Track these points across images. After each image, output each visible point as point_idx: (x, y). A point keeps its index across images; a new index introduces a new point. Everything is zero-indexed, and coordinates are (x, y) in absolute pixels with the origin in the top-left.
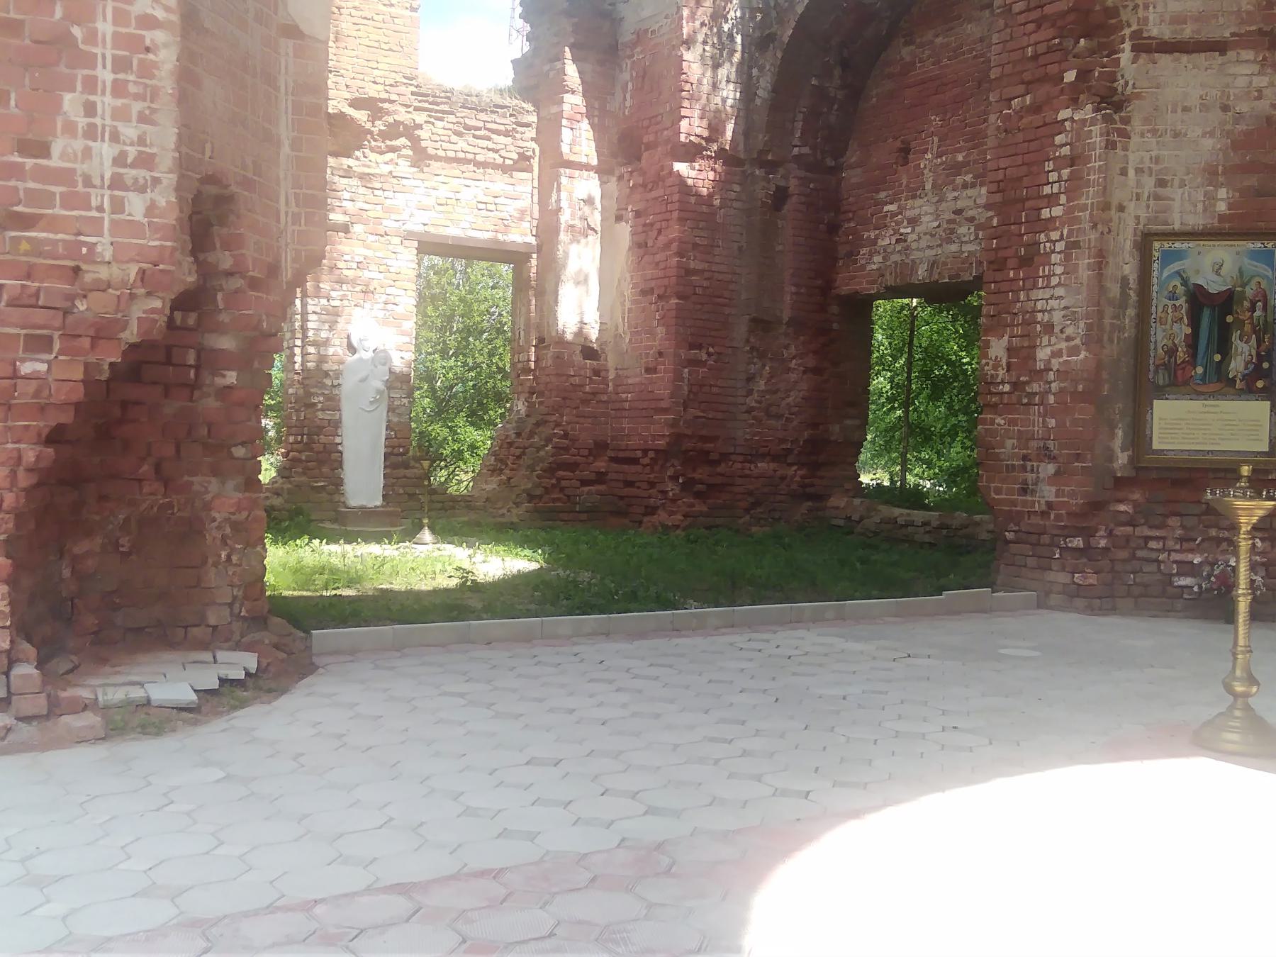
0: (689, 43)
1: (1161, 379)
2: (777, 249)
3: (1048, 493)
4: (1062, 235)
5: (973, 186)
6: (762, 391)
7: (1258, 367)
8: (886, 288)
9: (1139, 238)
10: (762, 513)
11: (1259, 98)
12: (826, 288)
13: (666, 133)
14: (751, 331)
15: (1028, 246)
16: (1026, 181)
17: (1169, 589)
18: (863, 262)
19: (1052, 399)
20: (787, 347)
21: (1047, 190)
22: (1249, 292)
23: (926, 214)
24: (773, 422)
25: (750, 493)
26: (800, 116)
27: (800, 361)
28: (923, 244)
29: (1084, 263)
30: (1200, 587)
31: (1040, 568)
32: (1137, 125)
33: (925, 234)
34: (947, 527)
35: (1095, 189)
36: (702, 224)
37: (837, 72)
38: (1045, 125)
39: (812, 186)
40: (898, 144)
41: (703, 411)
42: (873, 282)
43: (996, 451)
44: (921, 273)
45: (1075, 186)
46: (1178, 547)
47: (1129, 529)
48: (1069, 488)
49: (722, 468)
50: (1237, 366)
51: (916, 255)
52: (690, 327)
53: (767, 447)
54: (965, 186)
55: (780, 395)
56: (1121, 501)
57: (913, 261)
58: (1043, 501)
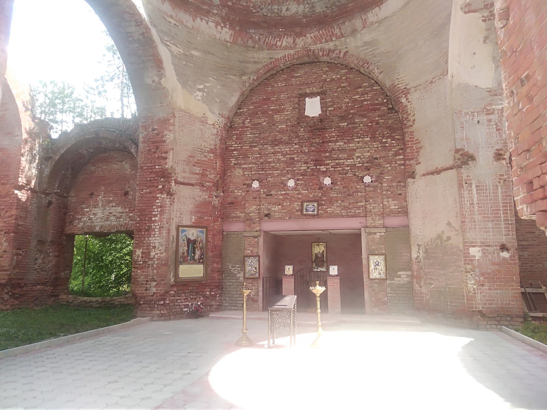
0: (22, 155)
1: (181, 260)
3: (154, 290)
4: (158, 225)
5: (115, 207)
7: (201, 257)
9: (176, 226)
11: (200, 197)
12: (62, 232)
13: (12, 181)
14: (38, 244)
15: (148, 226)
16: (147, 210)
17: (182, 312)
18: (76, 224)
19: (155, 266)
20: (49, 249)
21: (154, 213)
22: (199, 240)
23: (99, 213)
24: (43, 273)
25: (35, 296)
26: (58, 181)
28: (98, 221)
29: (164, 232)
30: (190, 311)
31: (151, 310)
32: (176, 200)
34: (104, 301)
36: (24, 210)
37: (70, 170)
38: (153, 197)
39: (60, 201)
40: (89, 193)
41: (19, 270)
44: (97, 229)
45: (162, 213)
46: (184, 301)
47: (174, 298)
49: (24, 289)
50: (197, 257)
52: (18, 243)
54: (113, 206)
55: (46, 264)
56: (171, 291)
57: (94, 225)
58: (152, 292)
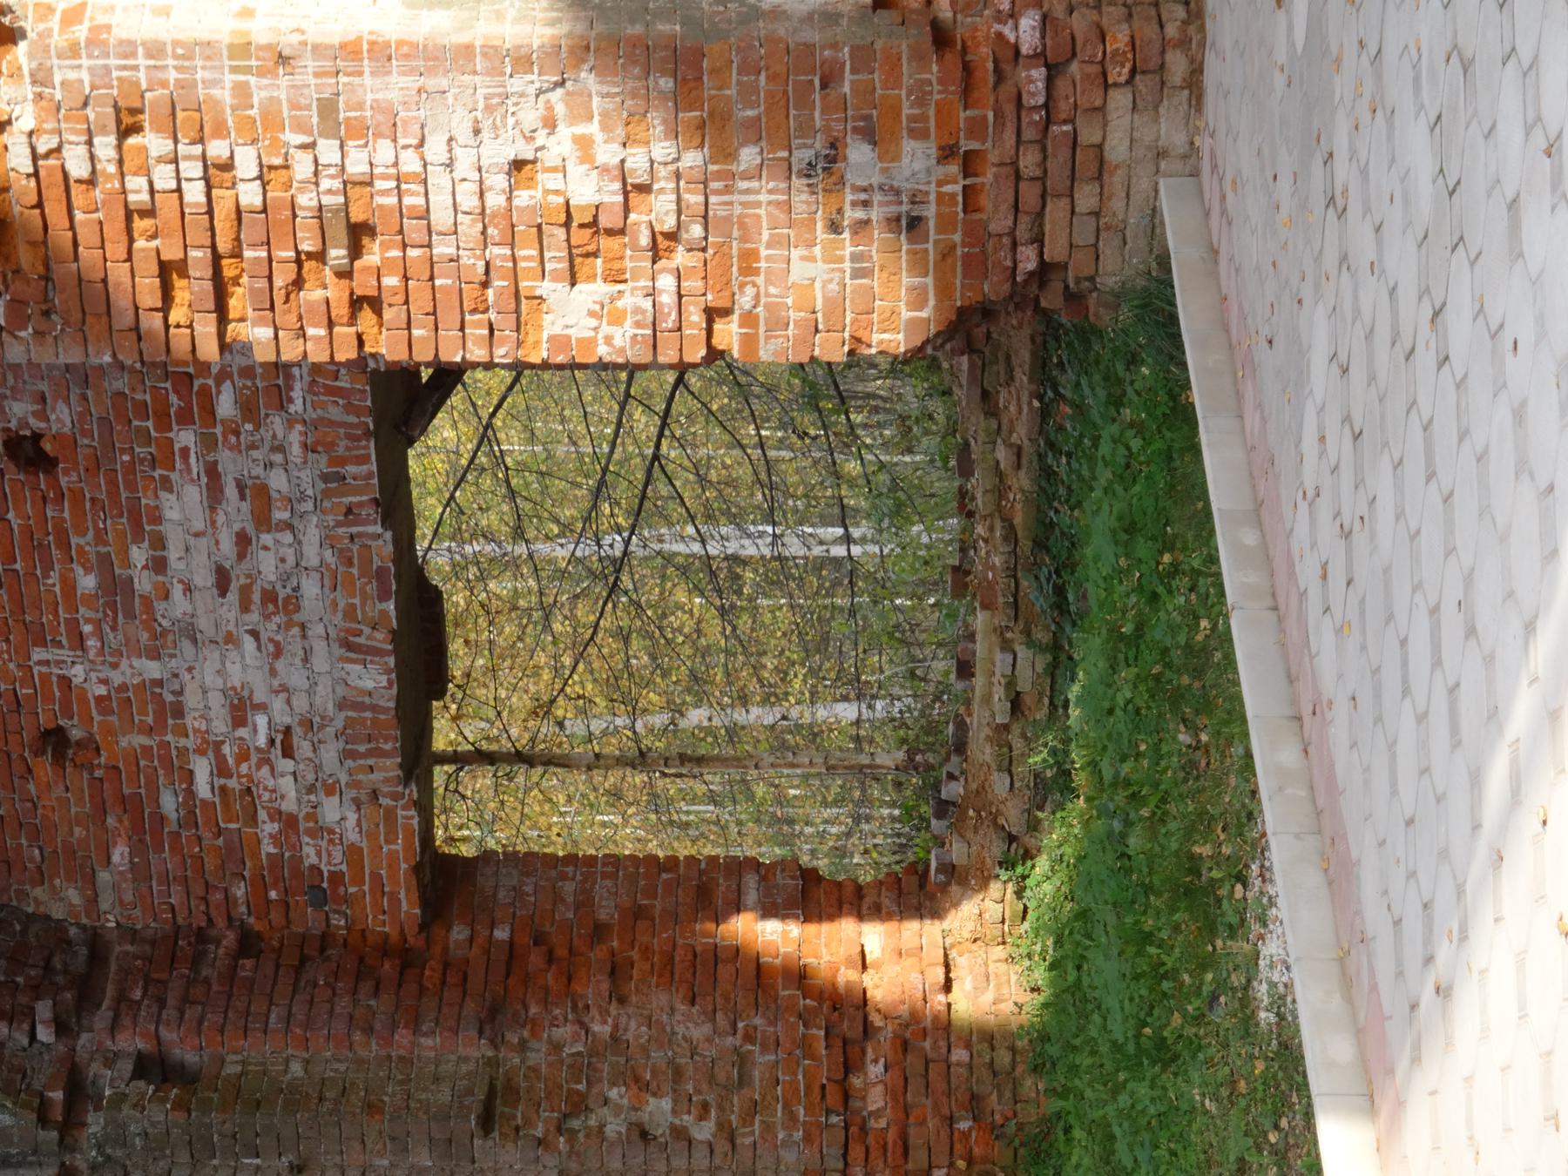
2: (301, 1074)
4: (303, 147)
5: (159, 542)
6: (675, 1101)
8: (406, 780)
10: (1000, 1096)
18: (338, 855)
20: (557, 1047)
27: (594, 1012)
33: (273, 672)
35: (199, 63)
42: (390, 815)
43: (819, 305)
48: (905, 104)
51: (325, 698)
53: (823, 1087)
57: (342, 705)
58: (941, 171)
